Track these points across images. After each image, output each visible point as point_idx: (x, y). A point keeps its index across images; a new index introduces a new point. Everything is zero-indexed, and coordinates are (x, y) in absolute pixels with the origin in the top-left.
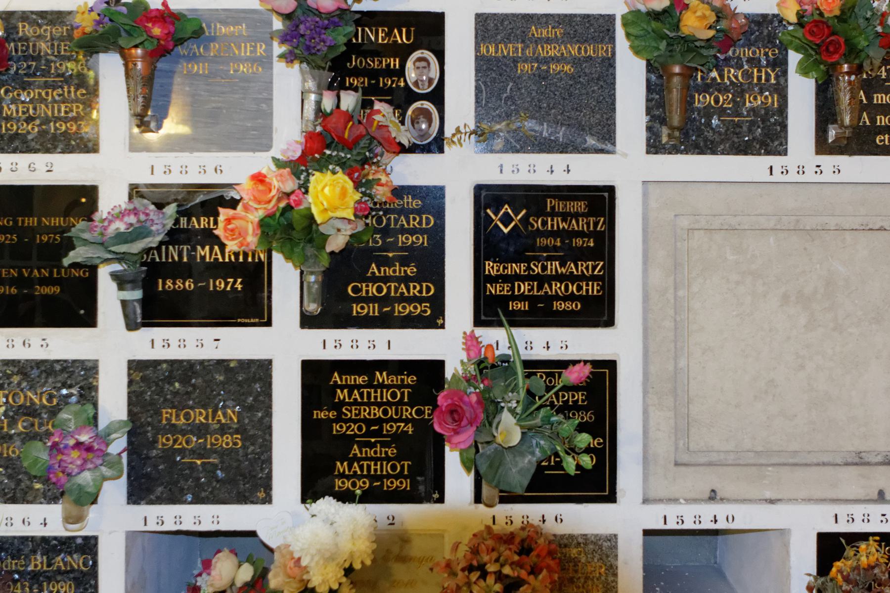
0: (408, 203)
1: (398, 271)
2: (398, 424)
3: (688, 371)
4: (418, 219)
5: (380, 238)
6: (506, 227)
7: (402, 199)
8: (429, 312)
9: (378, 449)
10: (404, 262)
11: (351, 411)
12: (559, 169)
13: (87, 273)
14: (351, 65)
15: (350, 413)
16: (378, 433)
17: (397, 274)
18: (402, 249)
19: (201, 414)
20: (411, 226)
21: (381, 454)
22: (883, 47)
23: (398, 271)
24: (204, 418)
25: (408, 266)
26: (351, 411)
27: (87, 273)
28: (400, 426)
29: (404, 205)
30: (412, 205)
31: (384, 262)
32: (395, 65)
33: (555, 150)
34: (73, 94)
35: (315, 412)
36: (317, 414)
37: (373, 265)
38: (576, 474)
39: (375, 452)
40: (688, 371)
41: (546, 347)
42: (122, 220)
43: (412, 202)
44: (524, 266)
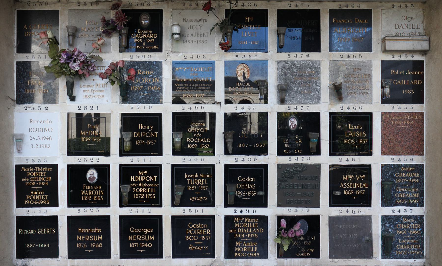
2: (135, 244)
8: (49, 203)
9: (38, 192)
10: (40, 190)
11: (32, 179)
12: (193, 211)
14: (407, 74)
15: (32, 179)
16: (37, 186)
18: (40, 186)
21: (39, 193)
22: (51, 58)
25: (41, 192)
26: (32, 179)
31: (35, 190)
32: (132, 178)
33: (278, 234)
34: (118, 22)
35: (27, 196)
37: (25, 25)
39: (37, 193)
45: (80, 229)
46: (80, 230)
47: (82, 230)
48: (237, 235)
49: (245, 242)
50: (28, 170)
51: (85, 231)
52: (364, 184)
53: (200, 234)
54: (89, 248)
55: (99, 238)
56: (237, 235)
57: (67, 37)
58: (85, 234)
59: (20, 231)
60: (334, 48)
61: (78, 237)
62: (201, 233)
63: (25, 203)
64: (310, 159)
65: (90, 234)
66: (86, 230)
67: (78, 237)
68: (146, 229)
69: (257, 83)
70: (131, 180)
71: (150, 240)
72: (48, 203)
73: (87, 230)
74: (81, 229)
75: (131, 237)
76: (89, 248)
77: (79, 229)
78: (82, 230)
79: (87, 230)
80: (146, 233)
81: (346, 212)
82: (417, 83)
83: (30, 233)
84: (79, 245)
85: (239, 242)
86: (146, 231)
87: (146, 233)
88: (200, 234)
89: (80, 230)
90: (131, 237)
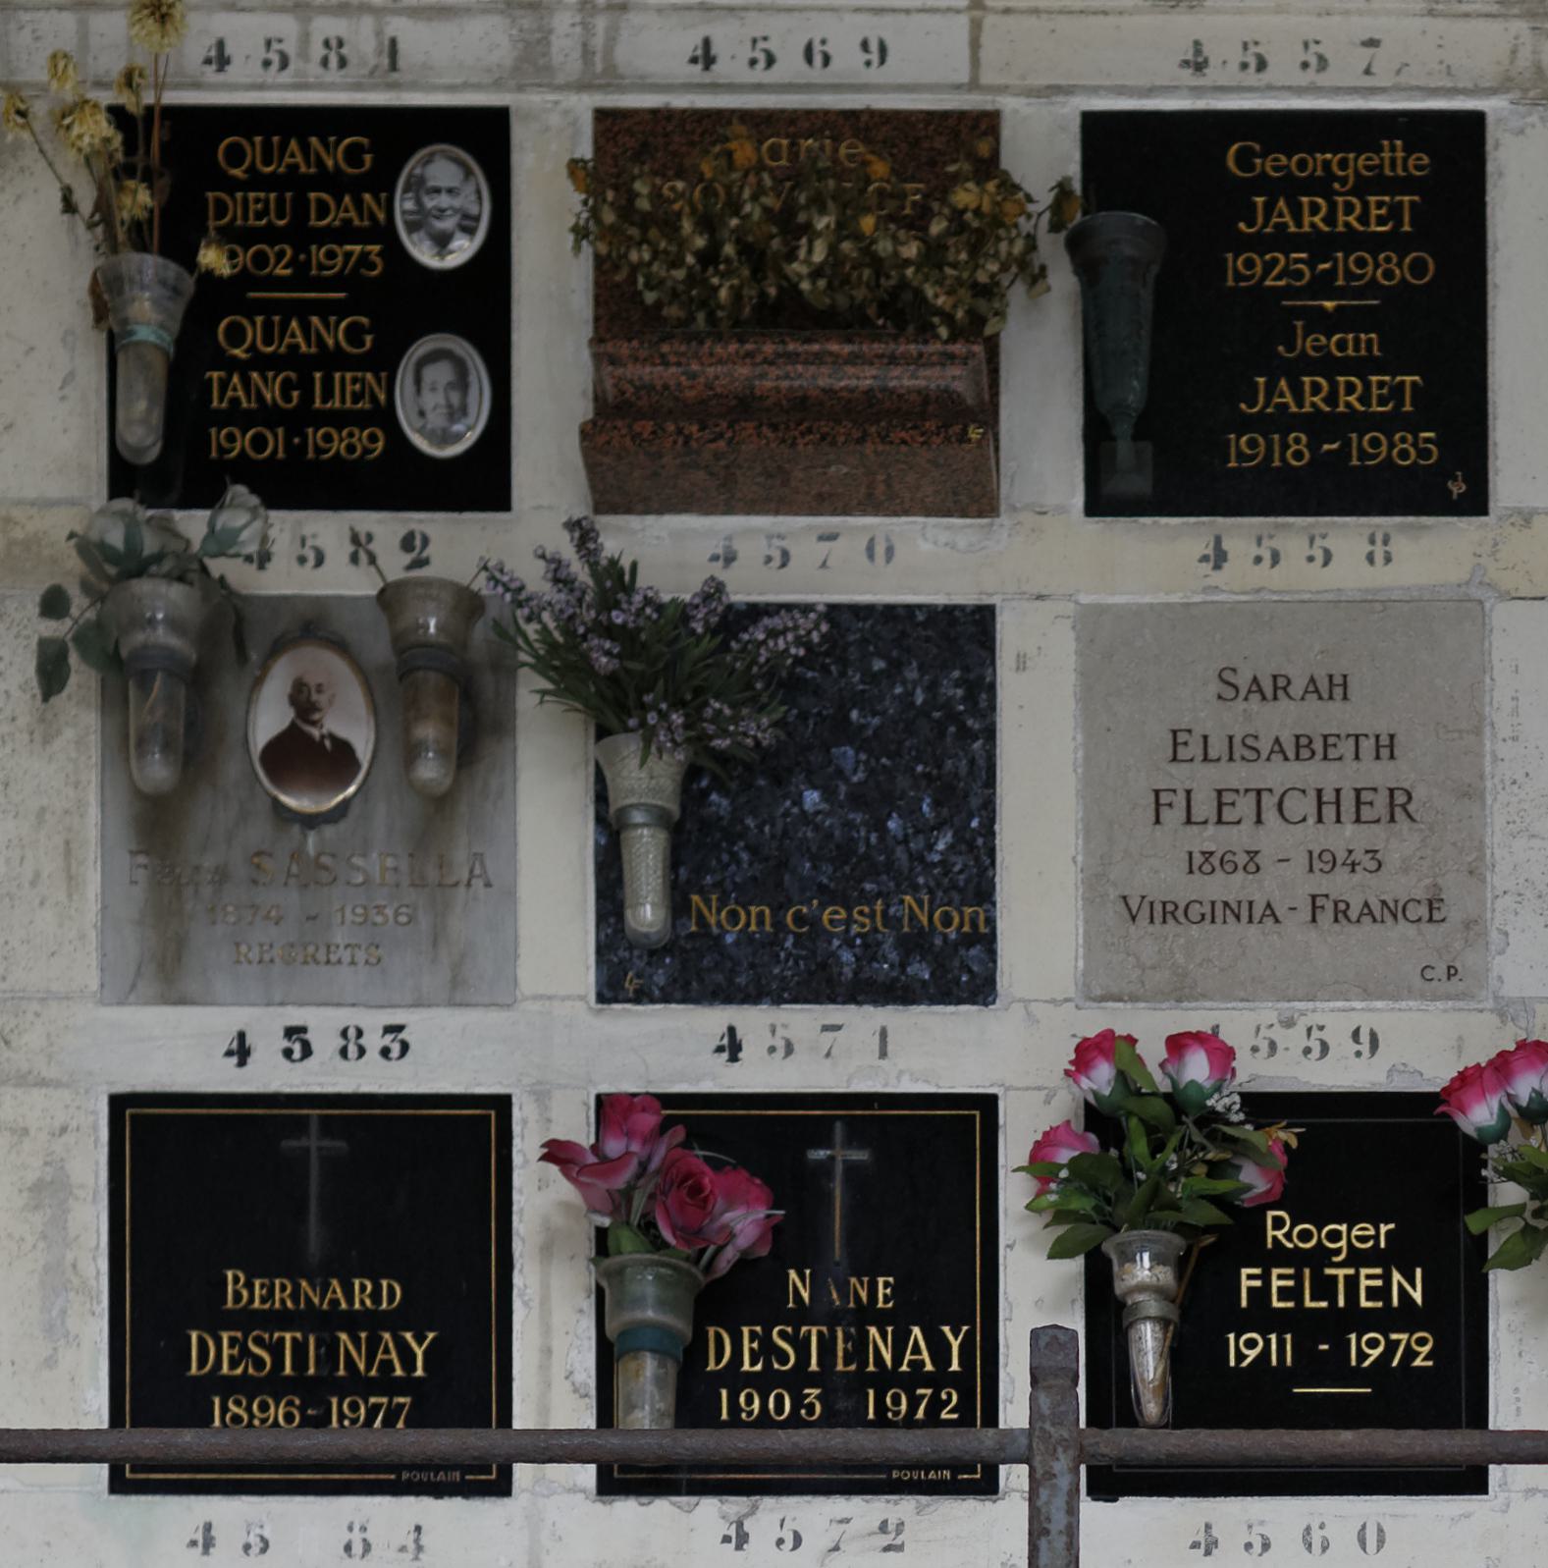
0: (1393, 161)
1: (1351, 345)
2: (1394, 1336)
3: (1467, 15)
4: (1358, 210)
5: (379, 254)
6: (974, 1116)
7: (1379, 150)
17: (1350, 352)
19: (1350, 389)
20: (1307, 229)
23: (1351, 345)
24: (1325, 400)
29: (1381, 166)
30: (1405, 168)
38: (1464, 481)
40: (1467, 15)
41: (411, 1546)
42: (974, 296)
43: (1405, 160)
44: (886, 1285)
50: (1357, 348)
51: (1376, 1237)
54: (1310, 1366)
59: (1270, 1233)
60: (121, 209)
61: (1417, 1296)
63: (1230, 283)
64: (1388, 559)
67: (1417, 1296)
68: (1343, 1228)
69: (232, 551)
70: (1288, 1337)
72: (1424, 454)
76: (1310, 1366)
78: (1355, 1232)
80: (1338, 1251)
81: (694, 60)
82: (371, 1296)
84: (1244, 1349)
86: (1343, 1243)
87: (1338, 1251)
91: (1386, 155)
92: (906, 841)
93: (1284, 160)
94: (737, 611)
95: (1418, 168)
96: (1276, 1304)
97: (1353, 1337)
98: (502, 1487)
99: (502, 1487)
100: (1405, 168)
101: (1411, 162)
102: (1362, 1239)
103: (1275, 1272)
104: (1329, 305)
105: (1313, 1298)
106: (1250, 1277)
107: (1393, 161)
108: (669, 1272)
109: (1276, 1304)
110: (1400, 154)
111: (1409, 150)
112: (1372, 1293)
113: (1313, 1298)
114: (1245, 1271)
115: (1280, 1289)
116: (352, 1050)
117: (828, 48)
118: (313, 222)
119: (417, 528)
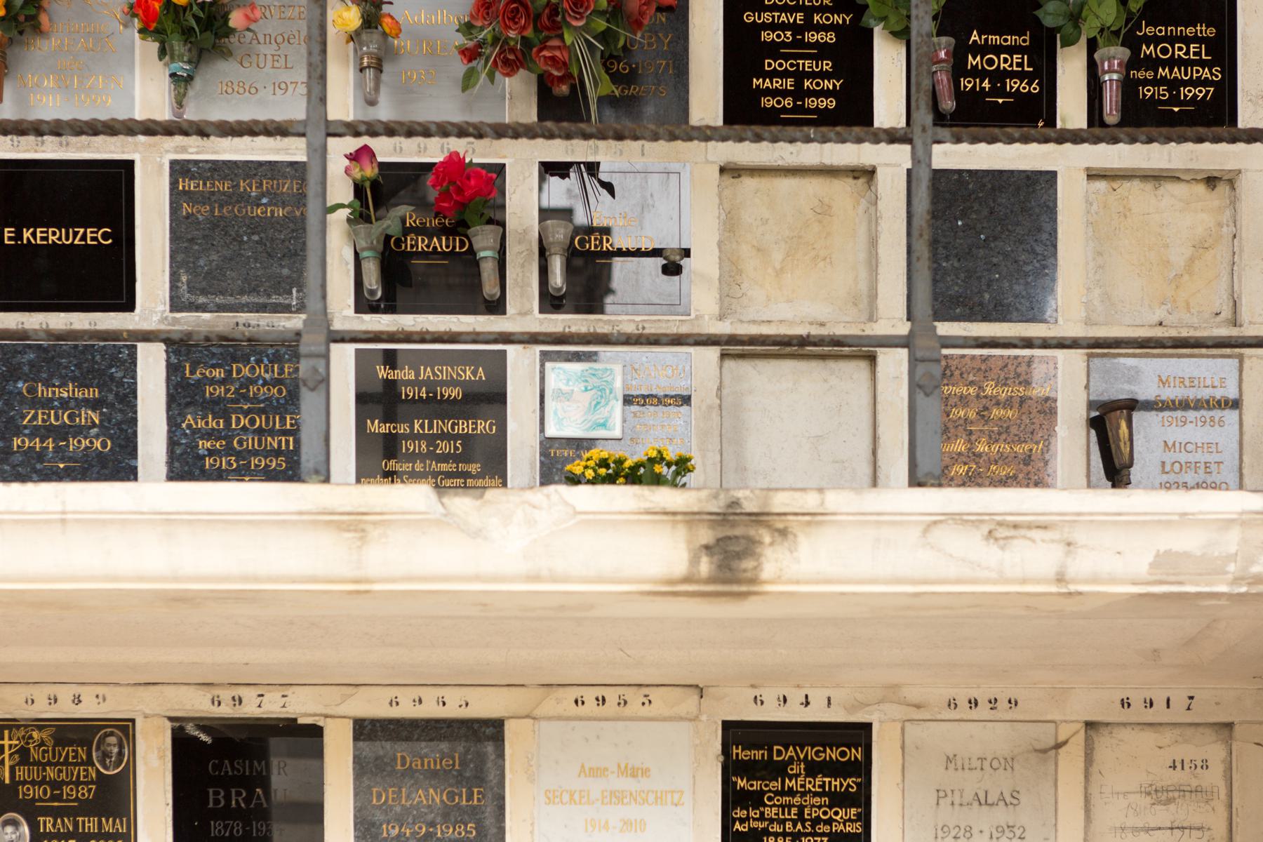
0: (1201, 31)
13: (494, 427)
27: (494, 427)
28: (80, 240)
30: (1206, 33)
36: (1134, 74)
43: (1206, 30)
45: (737, 748)
46: (737, 754)
47: (742, 751)
48: (215, 389)
49: (226, 761)
52: (1176, 69)
53: (426, 249)
55: (972, 64)
56: (215, 389)
57: (1231, 239)
58: (1156, 40)
62: (782, 85)
65: (1172, 40)
66: (753, 752)
71: (786, 789)
73: (755, 754)
74: (740, 751)
75: (855, 757)
77: (735, 751)
79: (755, 754)
83: (768, 87)
85: (111, 819)
88: (426, 249)
89: (737, 754)
90: (855, 757)
91: (1198, 28)
92: (194, 263)
93: (749, 753)
94: (167, 347)
95: (1211, 33)
96: (6, 242)
97: (1182, 89)
98: (908, 319)
99: (908, 319)
100: (1206, 33)
101: (1208, 32)
102: (745, 756)
103: (1015, 56)
104: (1000, 101)
105: (1028, 67)
106: (9, 232)
107: (1201, 31)
108: (945, 65)
109: (6, 242)
110: (1204, 28)
111: (1207, 27)
112: (775, 814)
113: (1028, 67)
114: (6, 230)
115: (1017, 63)
116: (1205, 767)
117: (763, 698)
118: (775, 758)
119: (1158, 455)
